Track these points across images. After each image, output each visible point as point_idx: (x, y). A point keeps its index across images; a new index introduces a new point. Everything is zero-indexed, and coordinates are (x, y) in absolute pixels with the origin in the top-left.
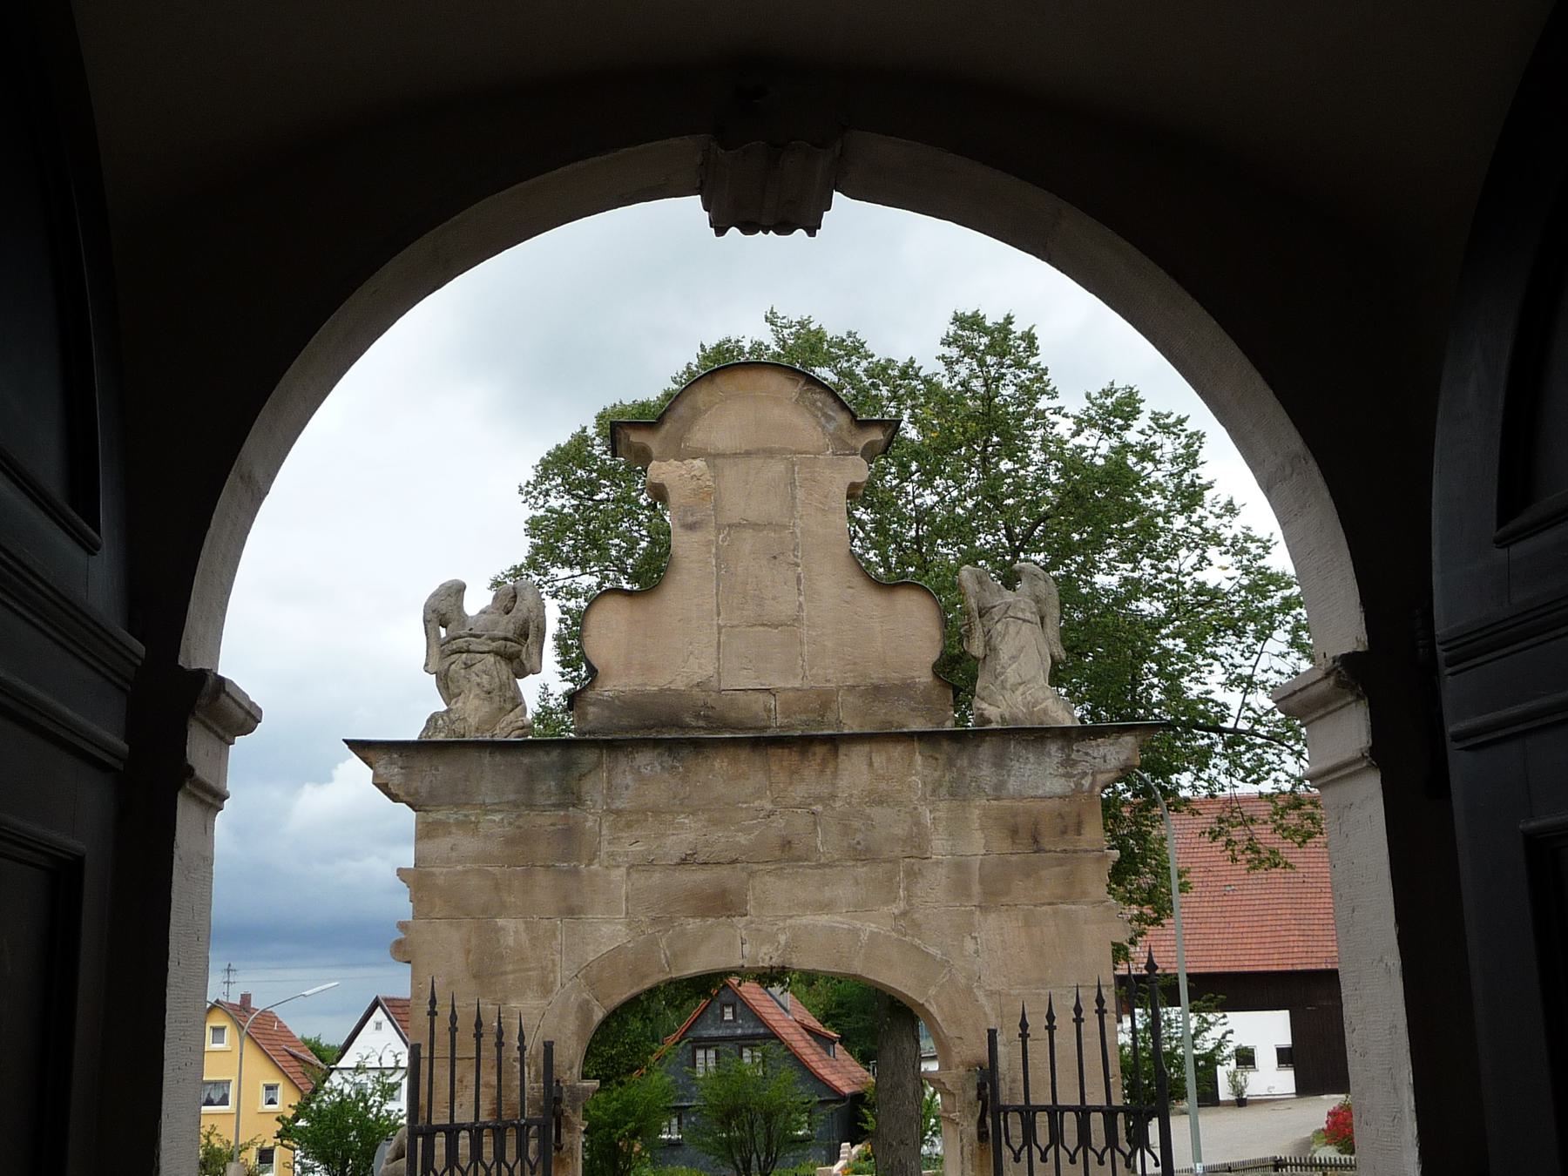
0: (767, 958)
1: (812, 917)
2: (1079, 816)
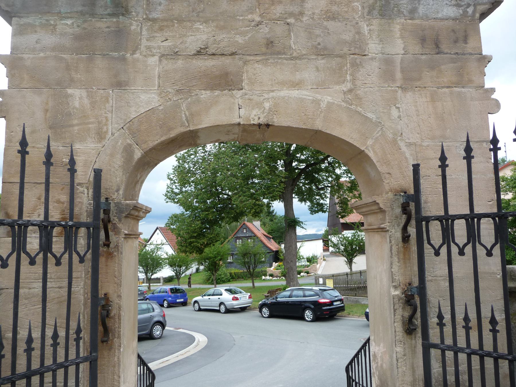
0: (256, 118)
1: (287, 91)
2: (466, 31)
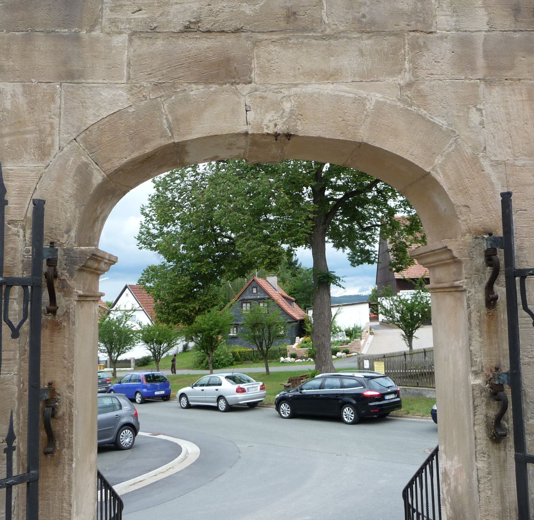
0: (272, 125)
1: (317, 86)
